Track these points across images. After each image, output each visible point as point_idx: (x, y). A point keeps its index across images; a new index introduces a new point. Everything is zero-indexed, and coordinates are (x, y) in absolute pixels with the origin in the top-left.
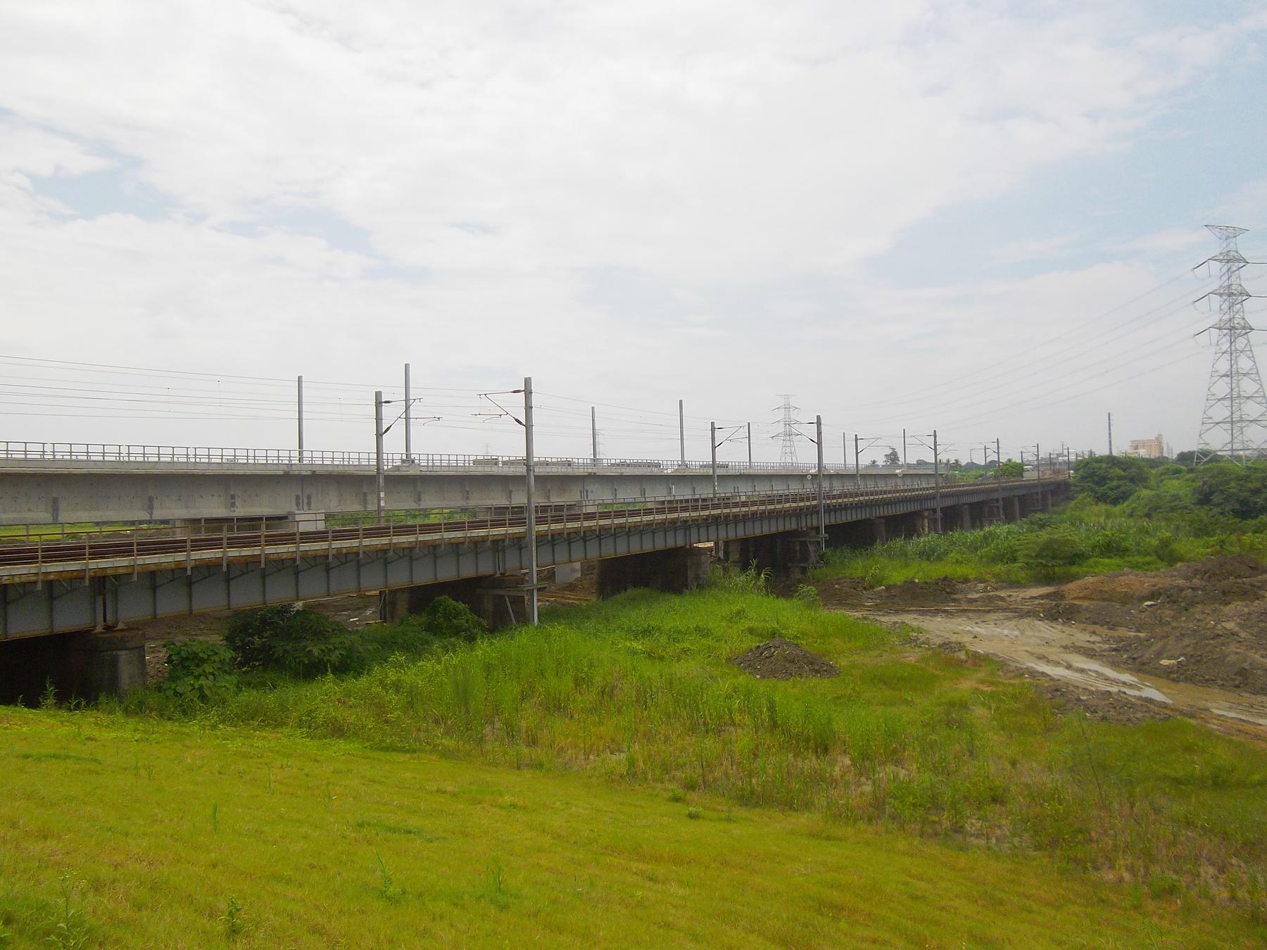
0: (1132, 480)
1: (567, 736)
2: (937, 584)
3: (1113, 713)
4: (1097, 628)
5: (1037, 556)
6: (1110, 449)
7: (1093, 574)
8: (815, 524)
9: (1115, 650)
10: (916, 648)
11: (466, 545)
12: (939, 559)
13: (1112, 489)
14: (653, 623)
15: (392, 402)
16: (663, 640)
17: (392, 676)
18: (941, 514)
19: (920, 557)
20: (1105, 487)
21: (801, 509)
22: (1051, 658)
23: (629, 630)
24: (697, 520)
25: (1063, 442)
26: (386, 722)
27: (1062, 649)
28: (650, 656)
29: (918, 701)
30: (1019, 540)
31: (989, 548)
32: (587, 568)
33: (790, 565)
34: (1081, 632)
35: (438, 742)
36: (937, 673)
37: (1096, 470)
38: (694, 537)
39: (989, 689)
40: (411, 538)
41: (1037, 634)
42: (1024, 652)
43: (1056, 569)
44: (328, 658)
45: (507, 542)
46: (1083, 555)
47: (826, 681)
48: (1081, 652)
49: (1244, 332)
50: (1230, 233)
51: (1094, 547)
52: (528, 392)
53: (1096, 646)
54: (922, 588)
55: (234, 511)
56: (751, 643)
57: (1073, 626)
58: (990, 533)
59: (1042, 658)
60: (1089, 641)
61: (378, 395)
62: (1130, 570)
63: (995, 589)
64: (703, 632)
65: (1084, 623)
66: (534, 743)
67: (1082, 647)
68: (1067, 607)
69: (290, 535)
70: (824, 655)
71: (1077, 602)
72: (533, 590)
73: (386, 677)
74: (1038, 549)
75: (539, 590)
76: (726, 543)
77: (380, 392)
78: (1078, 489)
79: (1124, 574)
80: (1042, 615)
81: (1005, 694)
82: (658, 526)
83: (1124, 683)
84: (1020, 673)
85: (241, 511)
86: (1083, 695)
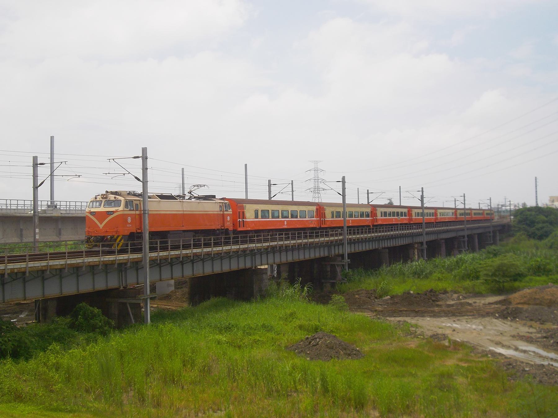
0: (551, 223)
1: (181, 401)
2: (426, 294)
3: (546, 378)
4: (533, 323)
5: (494, 275)
6: (537, 202)
7: (529, 287)
8: (341, 252)
9: (545, 337)
10: (415, 338)
11: (100, 267)
12: (426, 277)
13: (538, 229)
14: (233, 322)
15: (45, 164)
16: (240, 334)
17: (53, 359)
18: (426, 246)
19: (413, 276)
20: (534, 228)
21: (332, 242)
22: (504, 344)
23: (216, 327)
24: (261, 249)
25: (505, 197)
26: (52, 391)
27: (511, 338)
28: (231, 344)
29: (419, 374)
30: (480, 264)
31: (460, 270)
32: (179, 284)
33: (323, 281)
34: (523, 326)
35: (90, 405)
36: (430, 354)
38: (258, 261)
39: (466, 365)
40: (62, 262)
41: (495, 328)
42: (487, 340)
43: (505, 284)
44: (4, 347)
45: (129, 265)
46: (522, 274)
47: (355, 361)
48: (524, 339)
51: (529, 269)
52: (145, 158)
53: (533, 335)
54: (415, 297)
56: (301, 335)
57: (518, 322)
58: (461, 259)
59: (498, 344)
60: (528, 332)
61: (35, 158)
62: (552, 284)
63: (465, 298)
64: (267, 328)
65: (524, 320)
66: (158, 405)
67: (524, 336)
68: (514, 309)
69: (79, 252)
70: (353, 344)
71: (520, 306)
72: (147, 298)
73: (48, 361)
74: (493, 271)
75: (151, 299)
76: (279, 266)
78: (517, 229)
79: (549, 287)
80: (497, 315)
81: (476, 368)
82: (216, 256)
83: (552, 359)
84: (485, 354)
86: (527, 367)
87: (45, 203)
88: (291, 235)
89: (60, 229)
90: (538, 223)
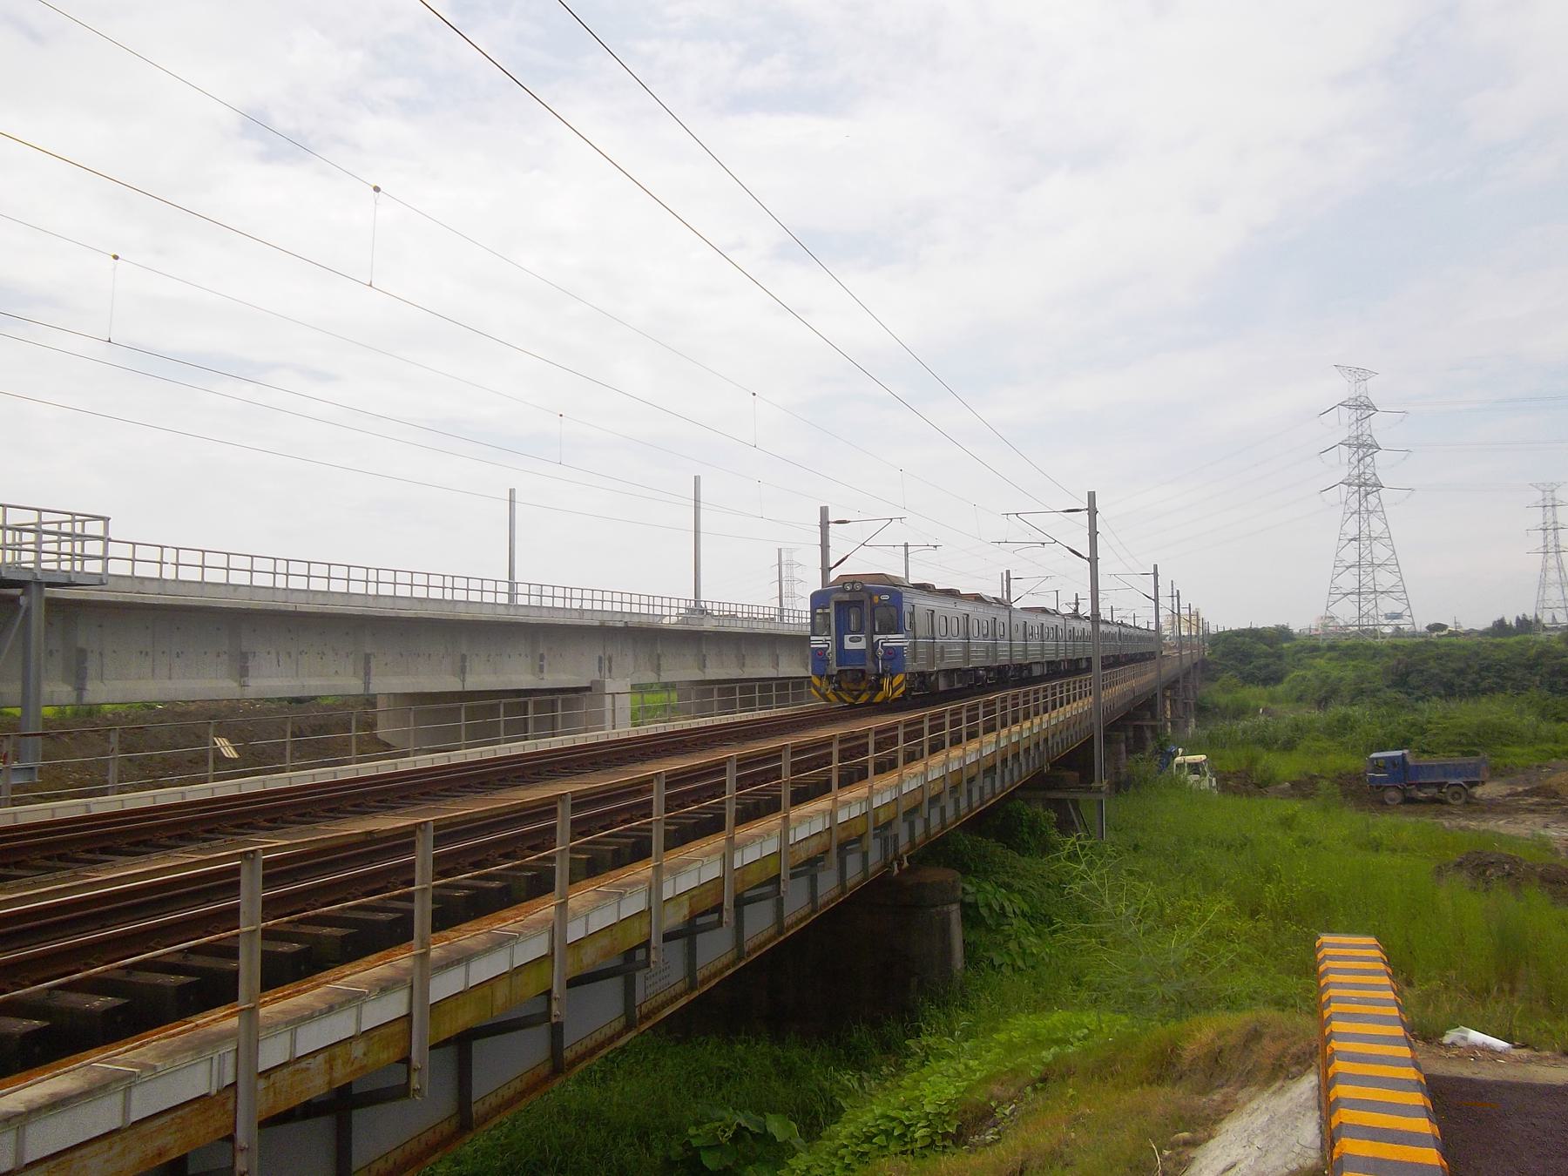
13: (1260, 669)
15: (1064, 511)
20: (1251, 666)
37: (1238, 646)
49: (1375, 489)
50: (1360, 374)
55: (543, 679)
77: (826, 508)
85: (550, 680)
87: (682, 604)
88: (735, 699)
89: (704, 656)
90: (1258, 656)
